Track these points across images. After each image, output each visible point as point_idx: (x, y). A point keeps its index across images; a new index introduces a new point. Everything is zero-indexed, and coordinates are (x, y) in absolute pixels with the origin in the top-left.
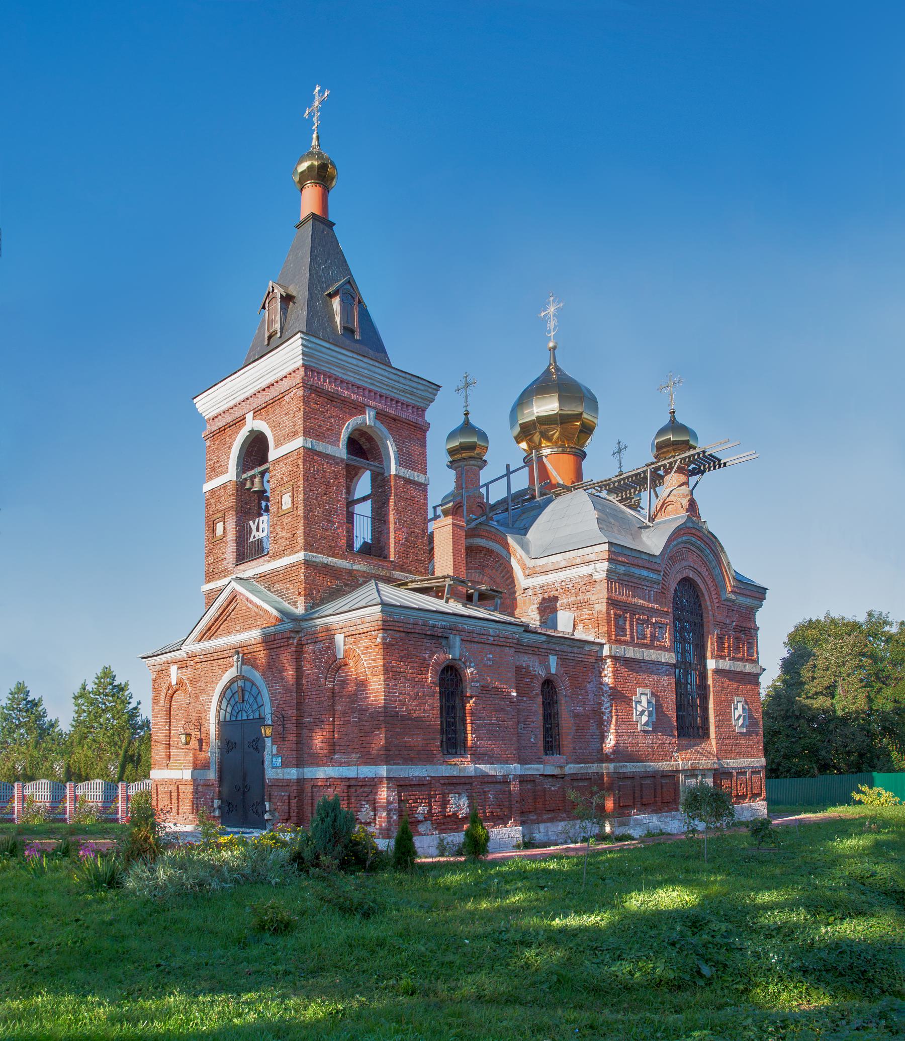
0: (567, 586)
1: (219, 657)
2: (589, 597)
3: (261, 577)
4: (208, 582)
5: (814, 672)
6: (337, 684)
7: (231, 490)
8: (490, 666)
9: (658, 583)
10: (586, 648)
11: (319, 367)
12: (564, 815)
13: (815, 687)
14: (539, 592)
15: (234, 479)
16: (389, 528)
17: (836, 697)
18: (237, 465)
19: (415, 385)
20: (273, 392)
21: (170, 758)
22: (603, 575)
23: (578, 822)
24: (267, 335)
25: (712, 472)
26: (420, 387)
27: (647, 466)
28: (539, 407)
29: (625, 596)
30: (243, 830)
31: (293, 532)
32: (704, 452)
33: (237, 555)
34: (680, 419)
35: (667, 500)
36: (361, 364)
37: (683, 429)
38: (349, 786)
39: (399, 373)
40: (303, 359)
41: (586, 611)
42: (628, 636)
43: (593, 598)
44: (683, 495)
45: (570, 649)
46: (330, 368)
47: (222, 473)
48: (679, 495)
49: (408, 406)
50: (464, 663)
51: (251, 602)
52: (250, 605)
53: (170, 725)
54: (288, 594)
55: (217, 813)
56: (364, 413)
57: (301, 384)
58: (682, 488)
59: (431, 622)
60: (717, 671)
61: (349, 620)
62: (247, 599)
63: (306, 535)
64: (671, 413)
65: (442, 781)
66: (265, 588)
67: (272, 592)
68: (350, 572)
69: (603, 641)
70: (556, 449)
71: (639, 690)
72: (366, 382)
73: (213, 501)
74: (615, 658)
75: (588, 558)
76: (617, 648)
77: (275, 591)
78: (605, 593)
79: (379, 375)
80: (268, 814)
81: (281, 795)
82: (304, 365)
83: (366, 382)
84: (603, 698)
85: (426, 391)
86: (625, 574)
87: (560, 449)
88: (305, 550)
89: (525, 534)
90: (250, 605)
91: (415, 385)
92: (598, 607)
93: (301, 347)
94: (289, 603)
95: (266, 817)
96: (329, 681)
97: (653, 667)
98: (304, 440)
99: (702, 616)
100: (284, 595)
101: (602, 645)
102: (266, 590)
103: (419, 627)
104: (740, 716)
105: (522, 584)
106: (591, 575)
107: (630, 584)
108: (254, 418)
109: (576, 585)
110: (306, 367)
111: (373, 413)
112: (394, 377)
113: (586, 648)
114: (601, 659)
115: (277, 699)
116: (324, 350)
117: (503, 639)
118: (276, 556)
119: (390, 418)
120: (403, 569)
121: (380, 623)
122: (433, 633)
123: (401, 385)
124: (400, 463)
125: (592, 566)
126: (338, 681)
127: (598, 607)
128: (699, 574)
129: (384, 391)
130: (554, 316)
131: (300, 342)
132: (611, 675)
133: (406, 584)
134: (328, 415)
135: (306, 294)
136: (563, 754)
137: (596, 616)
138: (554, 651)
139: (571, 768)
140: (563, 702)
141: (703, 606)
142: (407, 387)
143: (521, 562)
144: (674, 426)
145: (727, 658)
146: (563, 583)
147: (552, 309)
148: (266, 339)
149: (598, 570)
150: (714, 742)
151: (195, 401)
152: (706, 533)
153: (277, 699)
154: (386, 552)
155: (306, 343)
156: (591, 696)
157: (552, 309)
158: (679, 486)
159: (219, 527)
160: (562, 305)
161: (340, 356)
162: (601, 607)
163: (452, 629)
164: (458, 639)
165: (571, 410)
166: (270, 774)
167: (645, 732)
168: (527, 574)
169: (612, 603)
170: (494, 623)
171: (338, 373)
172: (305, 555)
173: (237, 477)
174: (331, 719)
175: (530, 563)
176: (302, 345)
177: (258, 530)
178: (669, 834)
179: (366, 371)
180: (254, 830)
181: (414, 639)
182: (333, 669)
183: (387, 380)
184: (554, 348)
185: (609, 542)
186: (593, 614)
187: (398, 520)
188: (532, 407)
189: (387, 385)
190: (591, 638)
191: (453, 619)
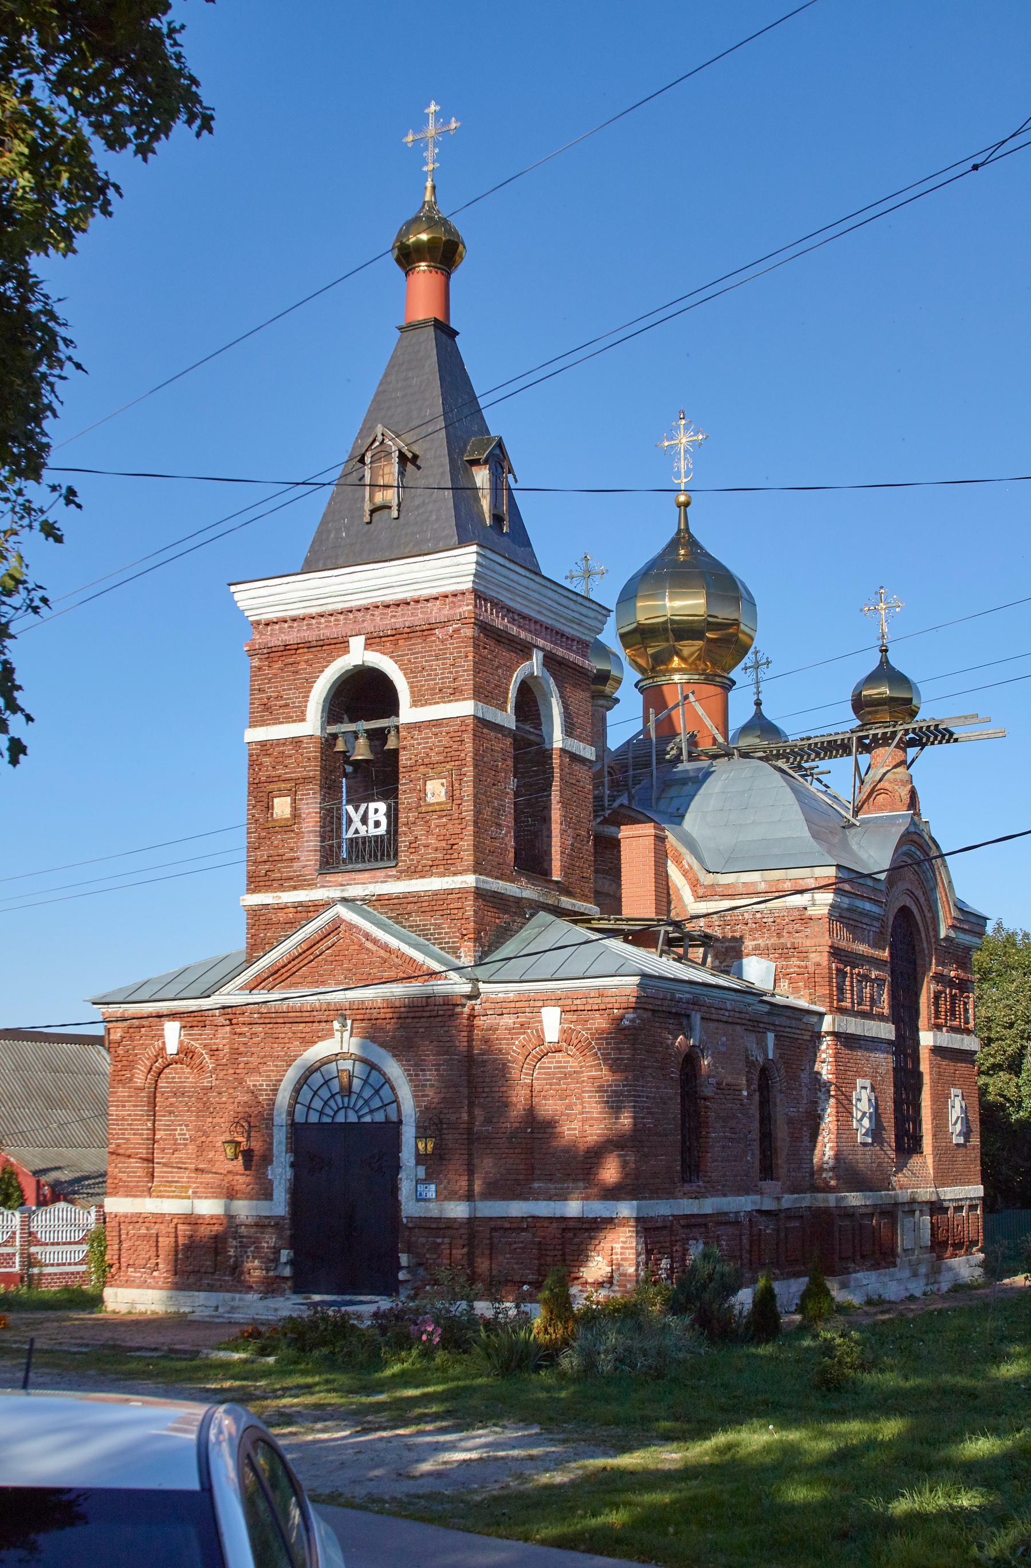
0: (765, 920)
1: (298, 1020)
2: (799, 940)
3: (381, 901)
4: (253, 891)
5: (989, 1029)
6: (537, 1079)
7: (312, 751)
8: (724, 1053)
9: (877, 919)
10: (804, 1020)
11: (486, 591)
12: (777, 1271)
13: (992, 1056)
14: (717, 923)
15: (318, 733)
16: (549, 830)
17: (1024, 1075)
18: (323, 712)
19: (584, 611)
20: (417, 617)
21: (153, 1176)
22: (825, 911)
23: (792, 1281)
24: (367, 507)
25: (937, 747)
26: (591, 614)
27: (853, 732)
28: (671, 600)
29: (846, 942)
30: (348, 1298)
31: (452, 842)
32: (937, 726)
33: (322, 856)
34: (896, 662)
35: (879, 786)
36: (532, 585)
37: (898, 679)
38: (564, 1230)
39: (571, 596)
40: (474, 582)
41: (795, 962)
42: (849, 1000)
43: (808, 942)
44: (901, 781)
45: (787, 1022)
46: (498, 593)
47: (289, 719)
48: (895, 780)
49: (573, 640)
50: (702, 1051)
51: (375, 941)
52: (369, 945)
53: (154, 1121)
54: (439, 934)
55: (287, 1272)
56: (530, 658)
57: (473, 620)
58: (898, 770)
59: (678, 995)
60: (937, 1051)
61: (575, 990)
62: (367, 936)
63: (477, 848)
64: (881, 651)
65: (682, 1222)
66: (389, 918)
67: (404, 927)
68: (518, 901)
69: (822, 1009)
70: (697, 677)
71: (859, 1082)
72: (533, 610)
73: (267, 760)
74: (836, 1035)
75: (803, 885)
76: (840, 1021)
77: (411, 926)
78: (827, 938)
79: (550, 599)
80: (404, 1271)
81: (435, 1242)
82: (475, 591)
83: (533, 610)
84: (819, 1094)
85: (596, 619)
86: (848, 909)
87: (702, 677)
88: (475, 872)
89: (680, 824)
90: (369, 945)
91: (584, 611)
92: (814, 957)
93: (474, 566)
94: (442, 949)
95: (402, 1276)
96: (526, 1074)
97: (872, 1043)
98: (476, 705)
99: (915, 964)
100: (431, 934)
101: (821, 1015)
102: (390, 922)
103: (666, 1003)
104: (958, 1118)
105: (689, 908)
106: (805, 909)
107: (851, 922)
108: (368, 646)
109: (778, 921)
110: (479, 595)
111: (541, 654)
112: (565, 602)
113: (804, 1020)
114: (818, 1037)
115: (427, 1096)
116: (498, 568)
117: (737, 1015)
118: (413, 872)
119: (555, 661)
120: (569, 894)
121: (634, 1000)
122: (679, 1010)
123: (570, 612)
124: (569, 730)
125: (807, 896)
126: (539, 1074)
127: (814, 957)
128: (916, 900)
129: (550, 622)
130: (686, 451)
131: (474, 558)
132: (831, 1059)
133: (589, 921)
134: (496, 664)
135: (446, 460)
136: (777, 1179)
137: (811, 970)
138: (774, 1027)
139: (788, 1201)
140: (778, 1100)
141: (917, 948)
142: (576, 615)
143: (690, 875)
144: (885, 673)
145: (944, 1029)
146: (758, 915)
147: (684, 440)
148: (368, 513)
149: (817, 902)
150: (930, 1160)
151: (233, 588)
152: (927, 838)
153: (427, 1096)
154: (545, 866)
155: (481, 560)
156: (805, 1092)
157: (684, 440)
158: (895, 767)
159: (282, 807)
160: (700, 437)
161: (513, 576)
162: (819, 958)
163: (696, 1003)
164: (698, 1016)
165: (724, 614)
166: (409, 1208)
167: (864, 1144)
168: (700, 895)
169: (836, 953)
170: (733, 993)
171: (506, 598)
172: (477, 880)
173: (323, 729)
174: (529, 1130)
175: (707, 879)
176: (477, 563)
177: (364, 820)
178: (889, 1302)
179: (537, 596)
180: (377, 1298)
181: (660, 1020)
182: (535, 1057)
183: (556, 606)
184: (687, 504)
185: (838, 866)
186: (806, 967)
187: (566, 819)
188: (664, 599)
189: (555, 613)
190: (803, 1003)
191: (698, 990)
